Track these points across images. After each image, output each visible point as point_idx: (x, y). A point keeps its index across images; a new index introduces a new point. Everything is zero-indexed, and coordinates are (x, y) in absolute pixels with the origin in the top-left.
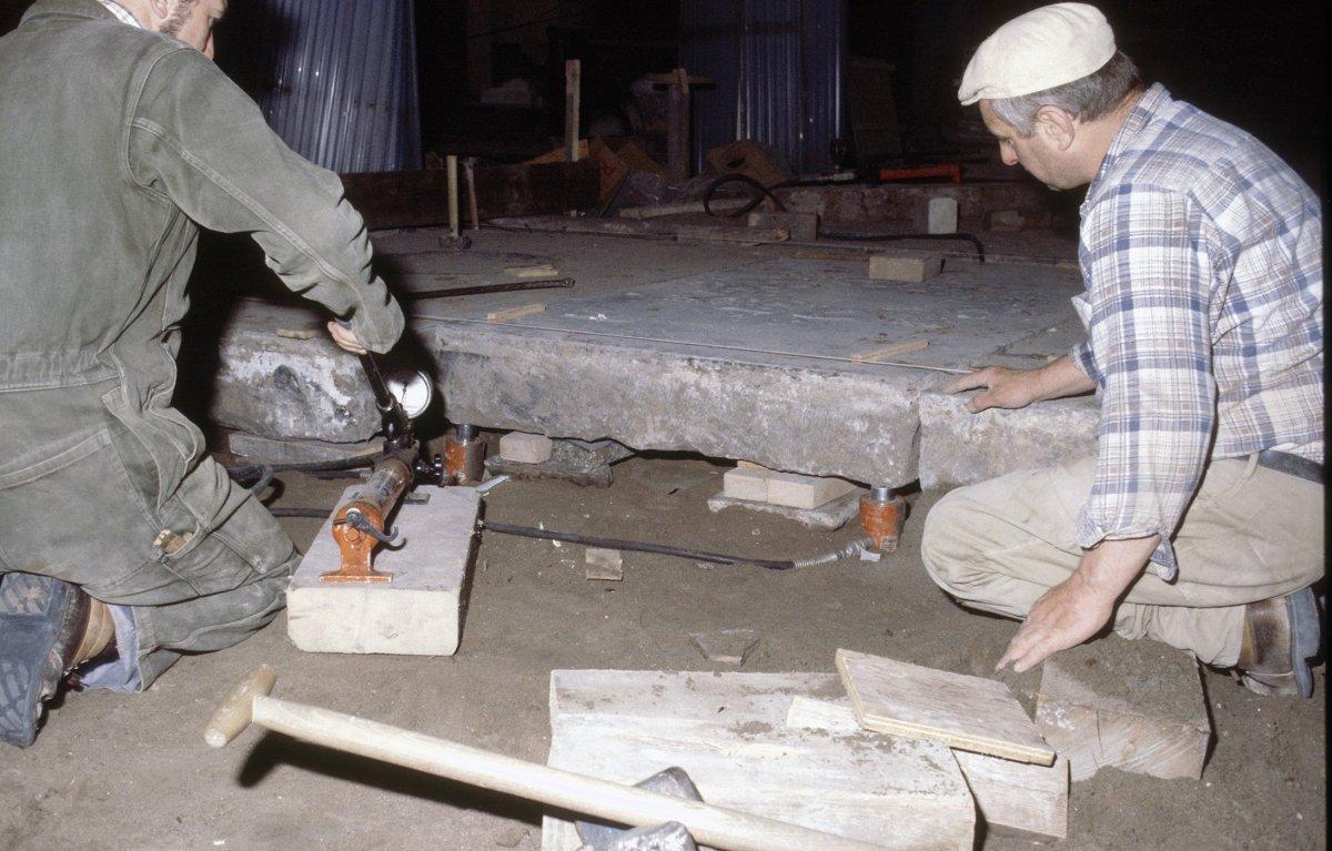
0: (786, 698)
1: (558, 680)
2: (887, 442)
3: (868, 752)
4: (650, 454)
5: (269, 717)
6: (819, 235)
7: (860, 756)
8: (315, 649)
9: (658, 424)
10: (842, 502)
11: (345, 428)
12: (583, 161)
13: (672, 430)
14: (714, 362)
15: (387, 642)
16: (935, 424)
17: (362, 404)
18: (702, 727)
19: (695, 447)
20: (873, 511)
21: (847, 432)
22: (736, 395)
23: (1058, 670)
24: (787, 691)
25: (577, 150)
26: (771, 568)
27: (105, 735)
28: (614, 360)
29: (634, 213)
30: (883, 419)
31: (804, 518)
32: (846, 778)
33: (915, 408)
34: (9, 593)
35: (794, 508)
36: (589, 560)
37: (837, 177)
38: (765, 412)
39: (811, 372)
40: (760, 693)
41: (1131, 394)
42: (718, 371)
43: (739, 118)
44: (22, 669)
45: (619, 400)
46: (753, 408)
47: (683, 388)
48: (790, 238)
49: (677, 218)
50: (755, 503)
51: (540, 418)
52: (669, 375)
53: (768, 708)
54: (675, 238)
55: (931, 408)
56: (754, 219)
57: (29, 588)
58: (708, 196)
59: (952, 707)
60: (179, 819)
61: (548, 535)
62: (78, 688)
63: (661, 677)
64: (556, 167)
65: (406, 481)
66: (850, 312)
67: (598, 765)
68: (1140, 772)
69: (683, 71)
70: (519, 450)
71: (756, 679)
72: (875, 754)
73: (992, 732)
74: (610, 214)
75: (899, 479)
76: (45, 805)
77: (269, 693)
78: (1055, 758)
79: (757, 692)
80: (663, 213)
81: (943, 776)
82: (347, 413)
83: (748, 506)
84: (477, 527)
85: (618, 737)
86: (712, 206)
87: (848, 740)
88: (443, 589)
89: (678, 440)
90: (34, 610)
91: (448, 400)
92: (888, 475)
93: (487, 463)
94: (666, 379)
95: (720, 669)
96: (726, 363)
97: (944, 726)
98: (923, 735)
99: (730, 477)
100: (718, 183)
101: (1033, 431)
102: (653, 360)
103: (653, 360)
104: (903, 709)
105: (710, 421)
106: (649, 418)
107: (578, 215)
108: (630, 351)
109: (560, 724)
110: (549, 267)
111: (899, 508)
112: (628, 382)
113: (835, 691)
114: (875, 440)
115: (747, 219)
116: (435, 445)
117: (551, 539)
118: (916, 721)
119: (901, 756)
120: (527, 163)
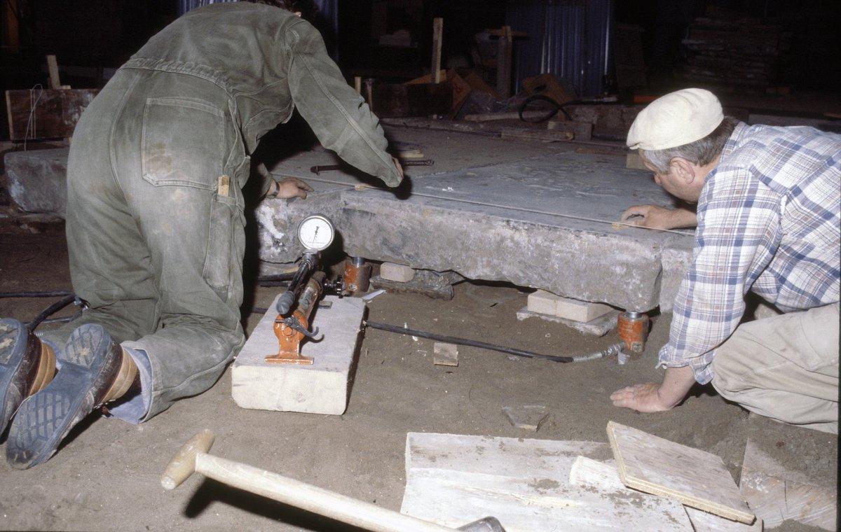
0: (568, 460)
1: (412, 439)
2: (638, 282)
3: (625, 506)
4: (479, 282)
5: (207, 469)
6: (593, 137)
7: (620, 510)
8: (249, 407)
9: (485, 263)
10: (606, 317)
11: (280, 254)
12: (443, 84)
13: (493, 268)
14: (524, 223)
15: (298, 405)
16: (672, 270)
17: (291, 239)
18: (511, 482)
19: (509, 279)
20: (627, 324)
22: (538, 246)
23: (757, 448)
24: (568, 454)
25: (439, 76)
26: (557, 361)
27: (103, 463)
28: (457, 220)
29: (474, 118)
30: (635, 266)
31: (580, 328)
32: (611, 526)
33: (658, 260)
34: (70, 347)
35: (574, 321)
36: (436, 351)
37: (606, 99)
39: (589, 233)
40: (550, 455)
41: (742, 222)
43: (543, 59)
44: (67, 401)
45: (460, 246)
46: (549, 255)
47: (503, 239)
48: (574, 139)
49: (497, 122)
50: (547, 315)
51: (407, 255)
52: (493, 231)
53: (554, 468)
54: (500, 136)
55: (670, 258)
56: (551, 125)
57: (83, 348)
58: (522, 109)
59: (686, 474)
60: (147, 527)
61: (410, 333)
62: (108, 415)
63: (483, 440)
64: (425, 88)
65: (318, 294)
66: (614, 190)
67: (437, 508)
68: (813, 525)
69: (509, 28)
70: (393, 273)
71: (548, 444)
72: (631, 509)
73: (712, 496)
74: (457, 119)
75: (646, 307)
76: (57, 513)
77: (208, 451)
78: (755, 520)
79: (548, 454)
80: (493, 119)
81: (679, 528)
82: (281, 244)
83: (543, 317)
84: (362, 326)
85: (451, 488)
86: (524, 116)
87: (612, 496)
88: (337, 370)
89: (498, 274)
90: (83, 363)
91: (347, 242)
92: (638, 304)
93: (371, 281)
94: (491, 234)
95: (523, 435)
96: (532, 224)
97: (681, 490)
98: (665, 494)
99: (531, 297)
100: (528, 101)
102: (483, 220)
103: (483, 220)
104: (653, 473)
105: (520, 262)
107: (438, 118)
108: (468, 214)
109: (411, 476)
110: (417, 152)
111: (644, 324)
112: (465, 233)
113: (605, 454)
115: (547, 123)
116: (336, 268)
117: (413, 335)
118: (661, 483)
119: (650, 511)
120: (405, 84)
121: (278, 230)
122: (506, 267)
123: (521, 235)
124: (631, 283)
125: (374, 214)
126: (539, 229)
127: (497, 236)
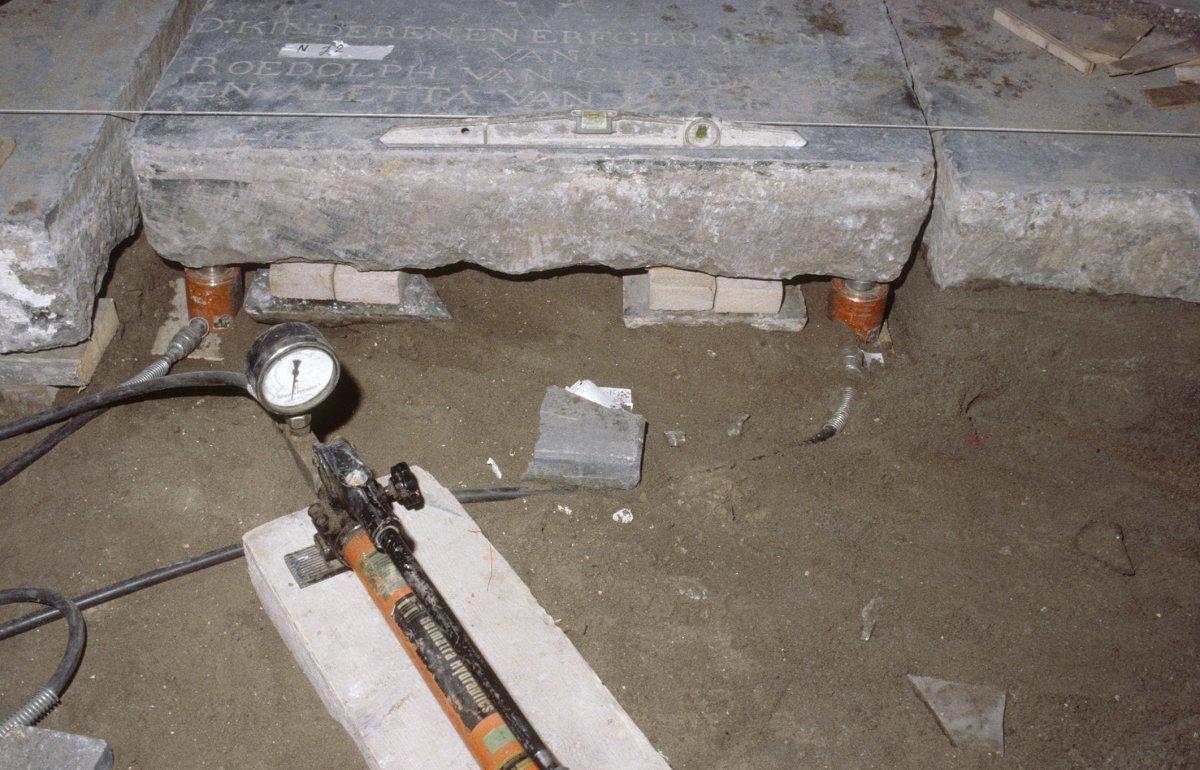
4: (532, 276)
9: (548, 244)
14: (639, 162)
16: (981, 223)
21: (835, 231)
22: (671, 201)
30: (888, 212)
31: (761, 324)
38: (716, 217)
42: (644, 174)
47: (588, 197)
52: (566, 185)
82: (53, 316)
94: (560, 189)
96: (657, 163)
101: (1109, 219)
106: (534, 239)
112: (500, 198)
114: (872, 236)
121: (36, 291)
122: (601, 245)
123: (633, 183)
124: (874, 241)
125: (246, 184)
126: (675, 170)
127: (573, 192)
